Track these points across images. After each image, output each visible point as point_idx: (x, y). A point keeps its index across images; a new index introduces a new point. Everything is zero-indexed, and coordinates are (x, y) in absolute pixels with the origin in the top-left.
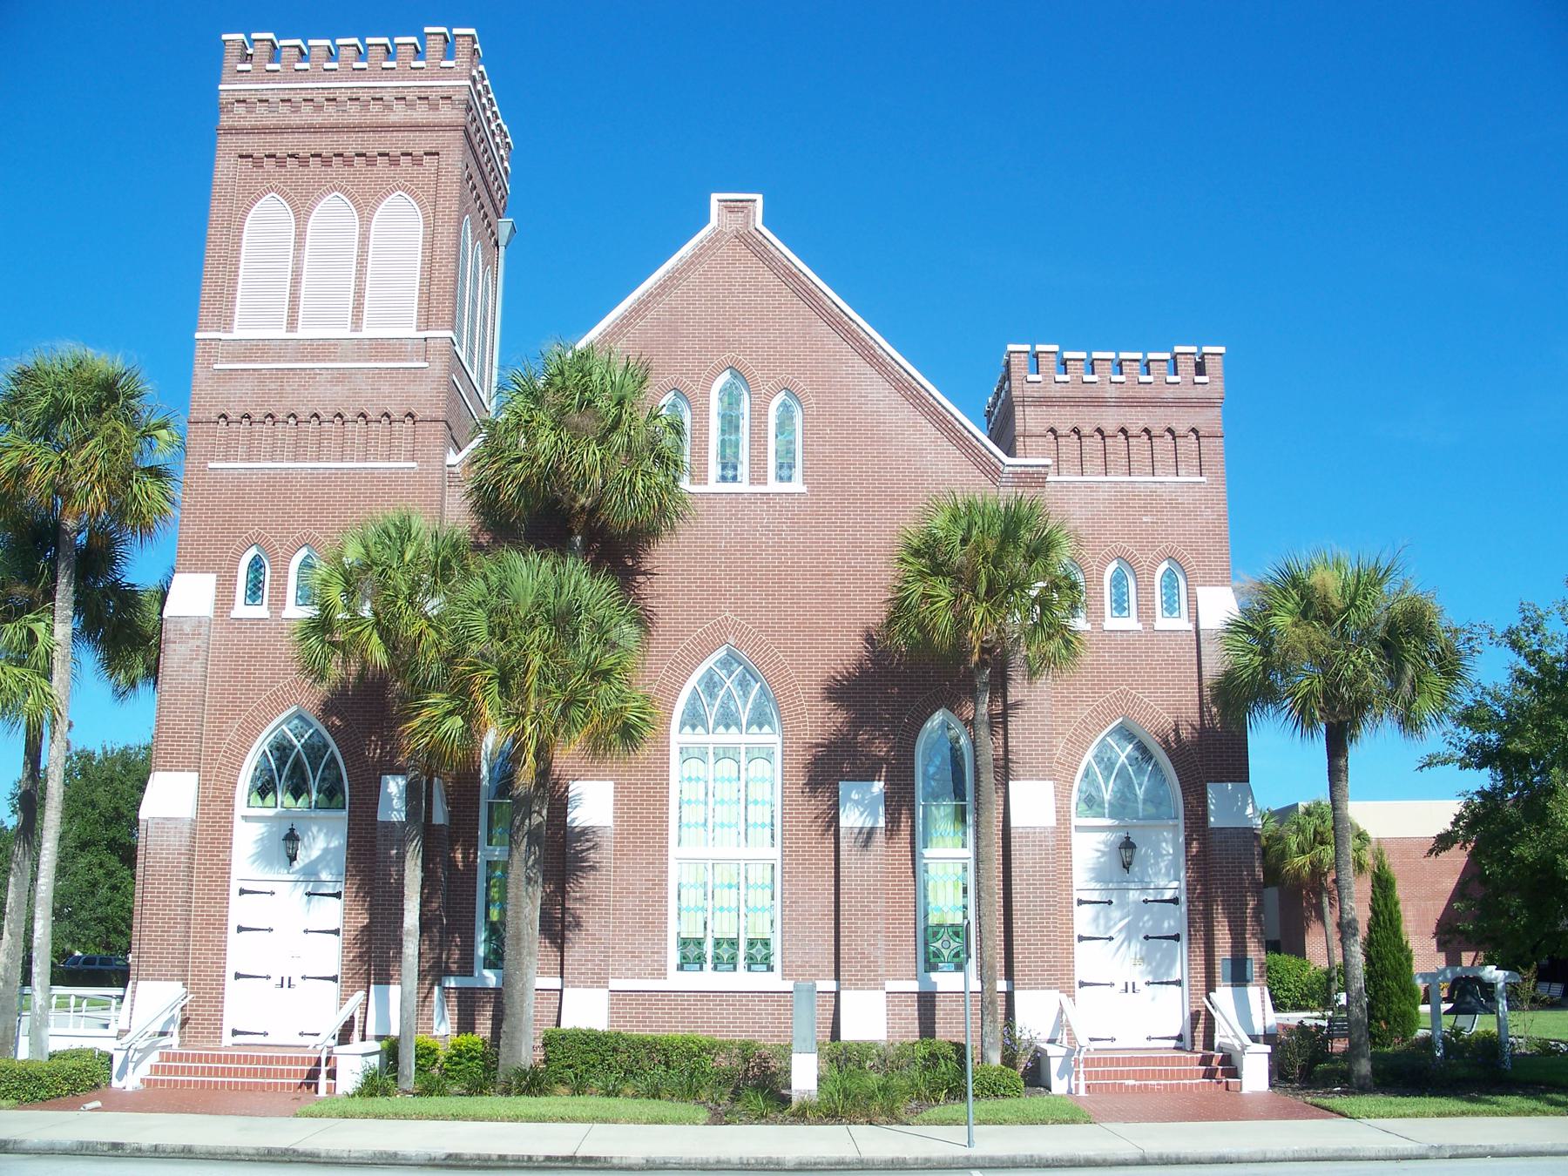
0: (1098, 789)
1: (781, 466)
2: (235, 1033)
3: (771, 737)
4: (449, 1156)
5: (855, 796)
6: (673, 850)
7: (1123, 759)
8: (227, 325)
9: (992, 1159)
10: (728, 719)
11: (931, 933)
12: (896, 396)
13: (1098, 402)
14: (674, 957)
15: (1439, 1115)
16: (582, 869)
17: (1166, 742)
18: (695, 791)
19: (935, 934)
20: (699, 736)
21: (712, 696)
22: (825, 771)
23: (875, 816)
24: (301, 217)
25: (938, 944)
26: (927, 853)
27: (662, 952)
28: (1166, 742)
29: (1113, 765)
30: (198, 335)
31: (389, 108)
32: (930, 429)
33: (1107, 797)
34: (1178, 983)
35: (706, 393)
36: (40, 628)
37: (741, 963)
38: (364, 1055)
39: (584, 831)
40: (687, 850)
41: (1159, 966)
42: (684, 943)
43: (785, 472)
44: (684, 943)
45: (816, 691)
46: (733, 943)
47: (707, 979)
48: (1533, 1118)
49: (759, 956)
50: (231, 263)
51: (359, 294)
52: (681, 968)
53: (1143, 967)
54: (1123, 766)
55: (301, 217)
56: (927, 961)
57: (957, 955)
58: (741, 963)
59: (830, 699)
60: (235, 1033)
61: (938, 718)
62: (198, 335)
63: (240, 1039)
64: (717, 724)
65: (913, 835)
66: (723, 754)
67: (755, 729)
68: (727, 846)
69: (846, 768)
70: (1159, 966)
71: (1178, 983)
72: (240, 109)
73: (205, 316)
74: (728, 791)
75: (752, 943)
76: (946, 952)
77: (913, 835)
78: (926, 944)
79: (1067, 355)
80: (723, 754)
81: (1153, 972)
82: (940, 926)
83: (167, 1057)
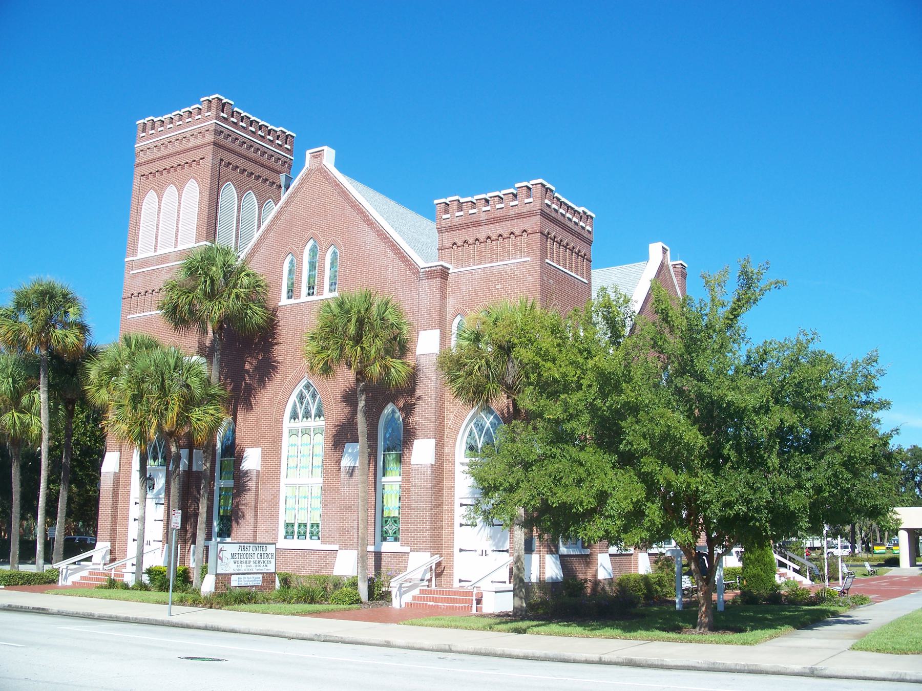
0: (476, 441)
1: (331, 285)
2: (460, 581)
3: (321, 422)
4: (9, 606)
5: (350, 451)
6: (283, 480)
7: (488, 425)
8: (135, 252)
9: (156, 621)
10: (307, 415)
11: (385, 521)
12: (378, 240)
13: (477, 224)
14: (282, 531)
15: (158, 602)
16: (245, 490)
17: (503, 414)
18: (293, 451)
19: (386, 521)
20: (301, 424)
21: (302, 403)
22: (342, 436)
23: (355, 460)
24: (160, 198)
25: (387, 527)
26: (384, 479)
27: (276, 530)
28: (503, 414)
29: (483, 428)
30: (126, 260)
31: (189, 140)
32: (391, 254)
33: (480, 446)
34: (507, 551)
35: (302, 253)
36: (36, 396)
37: (308, 535)
38: (496, 592)
39: (247, 472)
40: (291, 480)
41: (499, 541)
42: (287, 525)
43: (333, 287)
44: (287, 525)
45: (339, 397)
46: (305, 525)
47: (295, 543)
48: (693, 645)
49: (315, 532)
50: (199, 219)
51: (177, 230)
52: (285, 538)
53: (491, 542)
54: (488, 429)
55: (160, 198)
56: (382, 536)
57: (395, 533)
58: (308, 535)
59: (343, 401)
60: (460, 581)
61: (389, 408)
62: (126, 260)
63: (463, 584)
64: (315, 416)
65: (375, 470)
66: (306, 432)
67: (317, 418)
68: (305, 478)
69: (349, 436)
70: (499, 541)
71: (507, 551)
72: (142, 154)
73: (129, 251)
74: (306, 450)
75: (312, 526)
76: (390, 531)
77: (375, 470)
78: (382, 527)
79: (462, 201)
80: (306, 432)
81: (496, 545)
82: (388, 517)
83: (422, 591)
